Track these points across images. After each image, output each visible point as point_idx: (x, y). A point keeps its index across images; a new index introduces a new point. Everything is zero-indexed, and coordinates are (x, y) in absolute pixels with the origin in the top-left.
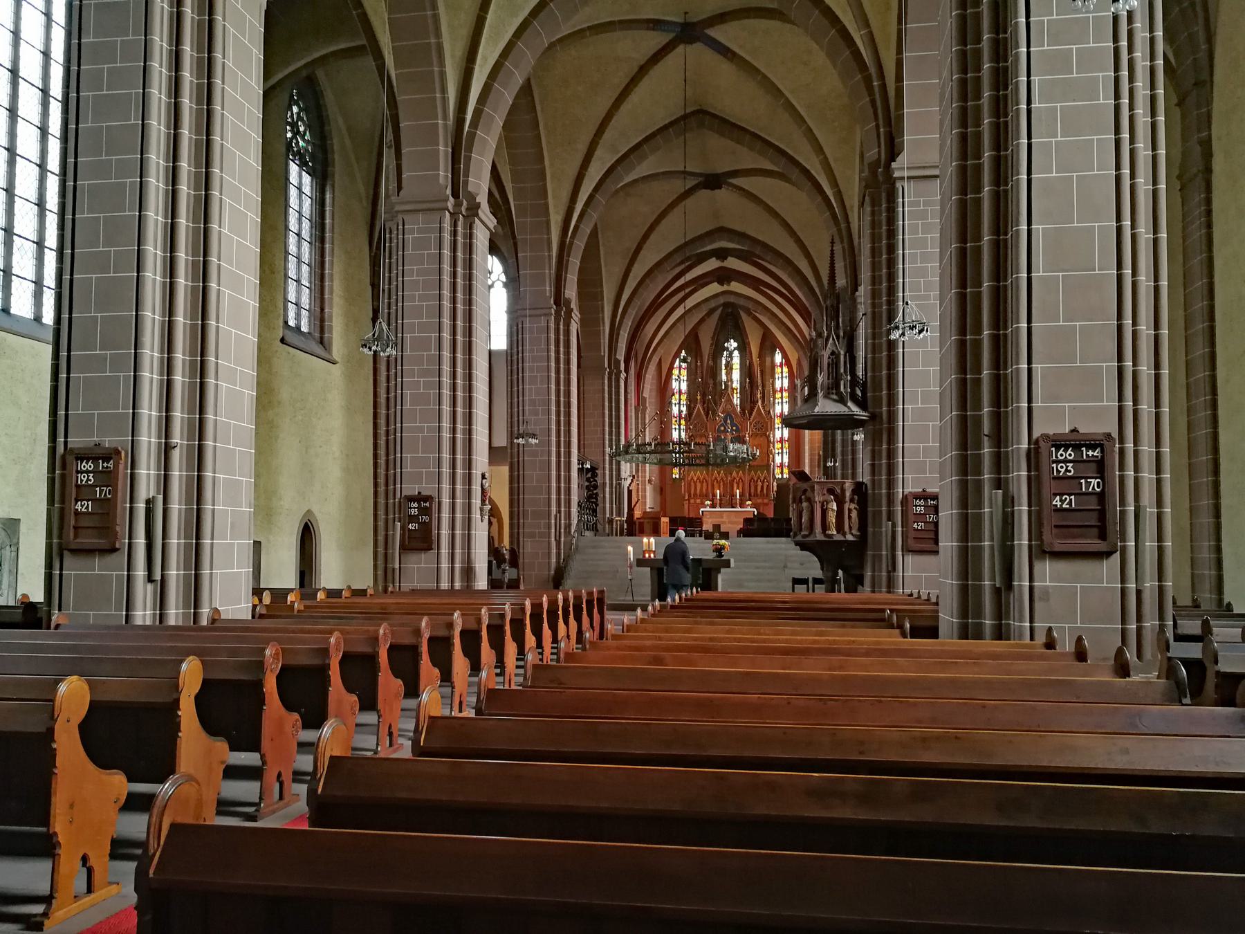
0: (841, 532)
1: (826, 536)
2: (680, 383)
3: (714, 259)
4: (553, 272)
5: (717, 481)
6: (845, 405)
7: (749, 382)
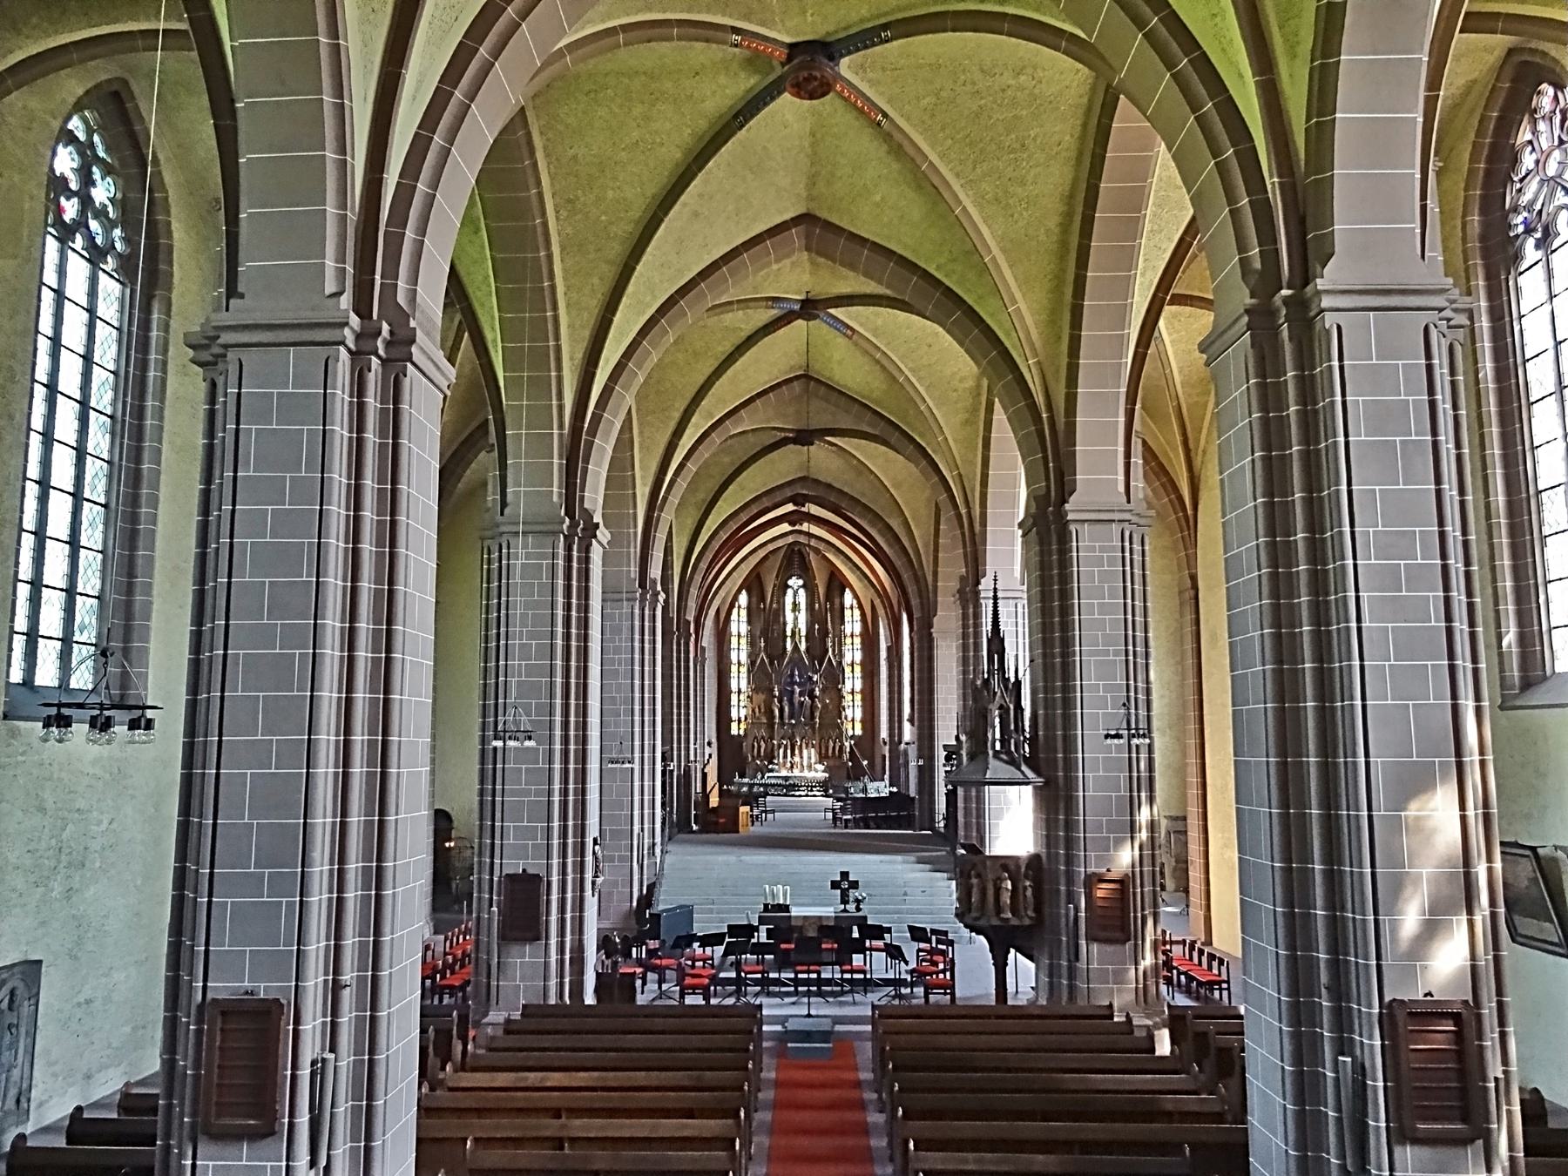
2: (739, 624)
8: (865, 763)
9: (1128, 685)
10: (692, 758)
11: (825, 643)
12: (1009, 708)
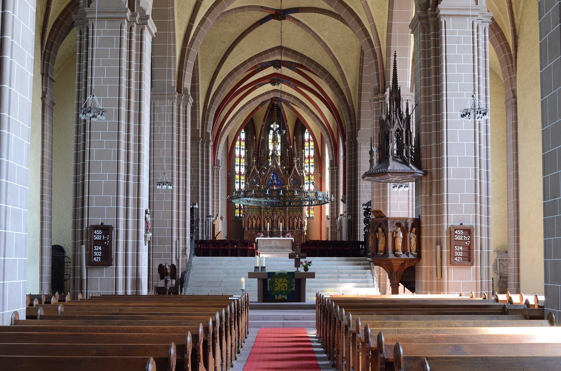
0: (405, 253)
1: (396, 255)
2: (240, 151)
3: (272, 67)
4: (177, 69)
6: (408, 166)
7: (289, 152)
9: (473, 32)
10: (211, 214)
12: (402, 130)
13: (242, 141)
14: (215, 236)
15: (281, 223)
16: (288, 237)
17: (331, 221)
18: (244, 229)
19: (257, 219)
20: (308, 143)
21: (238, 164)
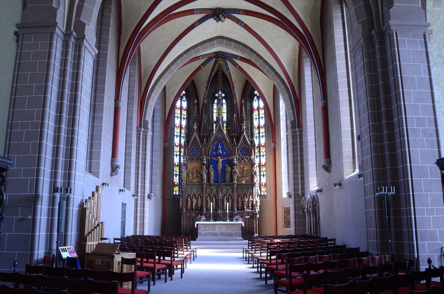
5: (210, 197)
8: (144, 249)
11: (241, 127)
13: (183, 110)
14: (86, 233)
15: (228, 203)
16: (237, 221)
17: (295, 200)
18: (182, 210)
19: (198, 198)
20: (257, 112)
21: (179, 134)
